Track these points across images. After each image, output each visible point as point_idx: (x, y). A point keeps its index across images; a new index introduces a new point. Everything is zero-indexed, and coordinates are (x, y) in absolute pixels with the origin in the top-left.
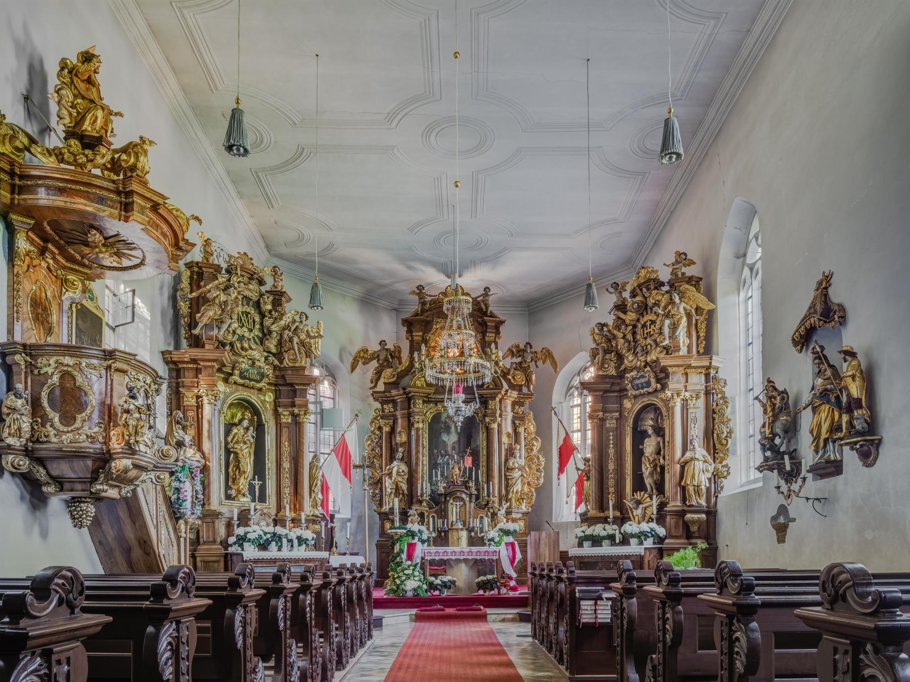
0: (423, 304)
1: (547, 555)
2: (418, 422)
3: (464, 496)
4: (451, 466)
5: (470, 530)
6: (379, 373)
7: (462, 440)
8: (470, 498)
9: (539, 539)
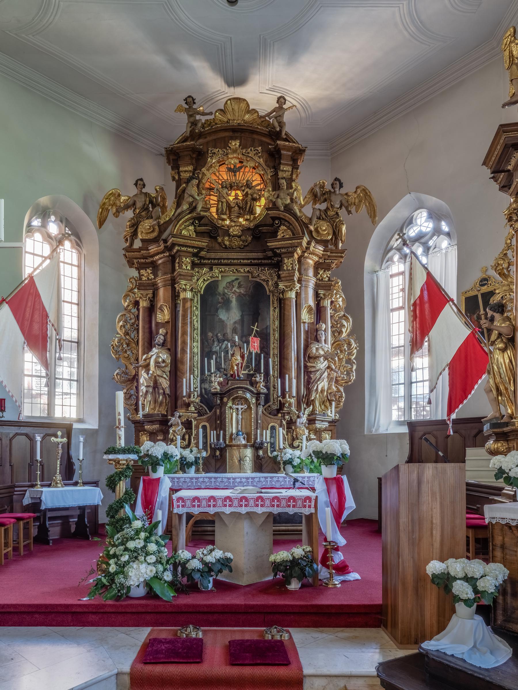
0: (194, 124)
1: (437, 520)
2: (185, 290)
3: (248, 396)
4: (230, 352)
5: (257, 447)
6: (135, 226)
7: (246, 318)
8: (257, 400)
9: (419, 483)
